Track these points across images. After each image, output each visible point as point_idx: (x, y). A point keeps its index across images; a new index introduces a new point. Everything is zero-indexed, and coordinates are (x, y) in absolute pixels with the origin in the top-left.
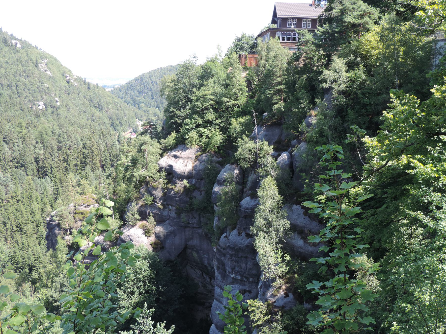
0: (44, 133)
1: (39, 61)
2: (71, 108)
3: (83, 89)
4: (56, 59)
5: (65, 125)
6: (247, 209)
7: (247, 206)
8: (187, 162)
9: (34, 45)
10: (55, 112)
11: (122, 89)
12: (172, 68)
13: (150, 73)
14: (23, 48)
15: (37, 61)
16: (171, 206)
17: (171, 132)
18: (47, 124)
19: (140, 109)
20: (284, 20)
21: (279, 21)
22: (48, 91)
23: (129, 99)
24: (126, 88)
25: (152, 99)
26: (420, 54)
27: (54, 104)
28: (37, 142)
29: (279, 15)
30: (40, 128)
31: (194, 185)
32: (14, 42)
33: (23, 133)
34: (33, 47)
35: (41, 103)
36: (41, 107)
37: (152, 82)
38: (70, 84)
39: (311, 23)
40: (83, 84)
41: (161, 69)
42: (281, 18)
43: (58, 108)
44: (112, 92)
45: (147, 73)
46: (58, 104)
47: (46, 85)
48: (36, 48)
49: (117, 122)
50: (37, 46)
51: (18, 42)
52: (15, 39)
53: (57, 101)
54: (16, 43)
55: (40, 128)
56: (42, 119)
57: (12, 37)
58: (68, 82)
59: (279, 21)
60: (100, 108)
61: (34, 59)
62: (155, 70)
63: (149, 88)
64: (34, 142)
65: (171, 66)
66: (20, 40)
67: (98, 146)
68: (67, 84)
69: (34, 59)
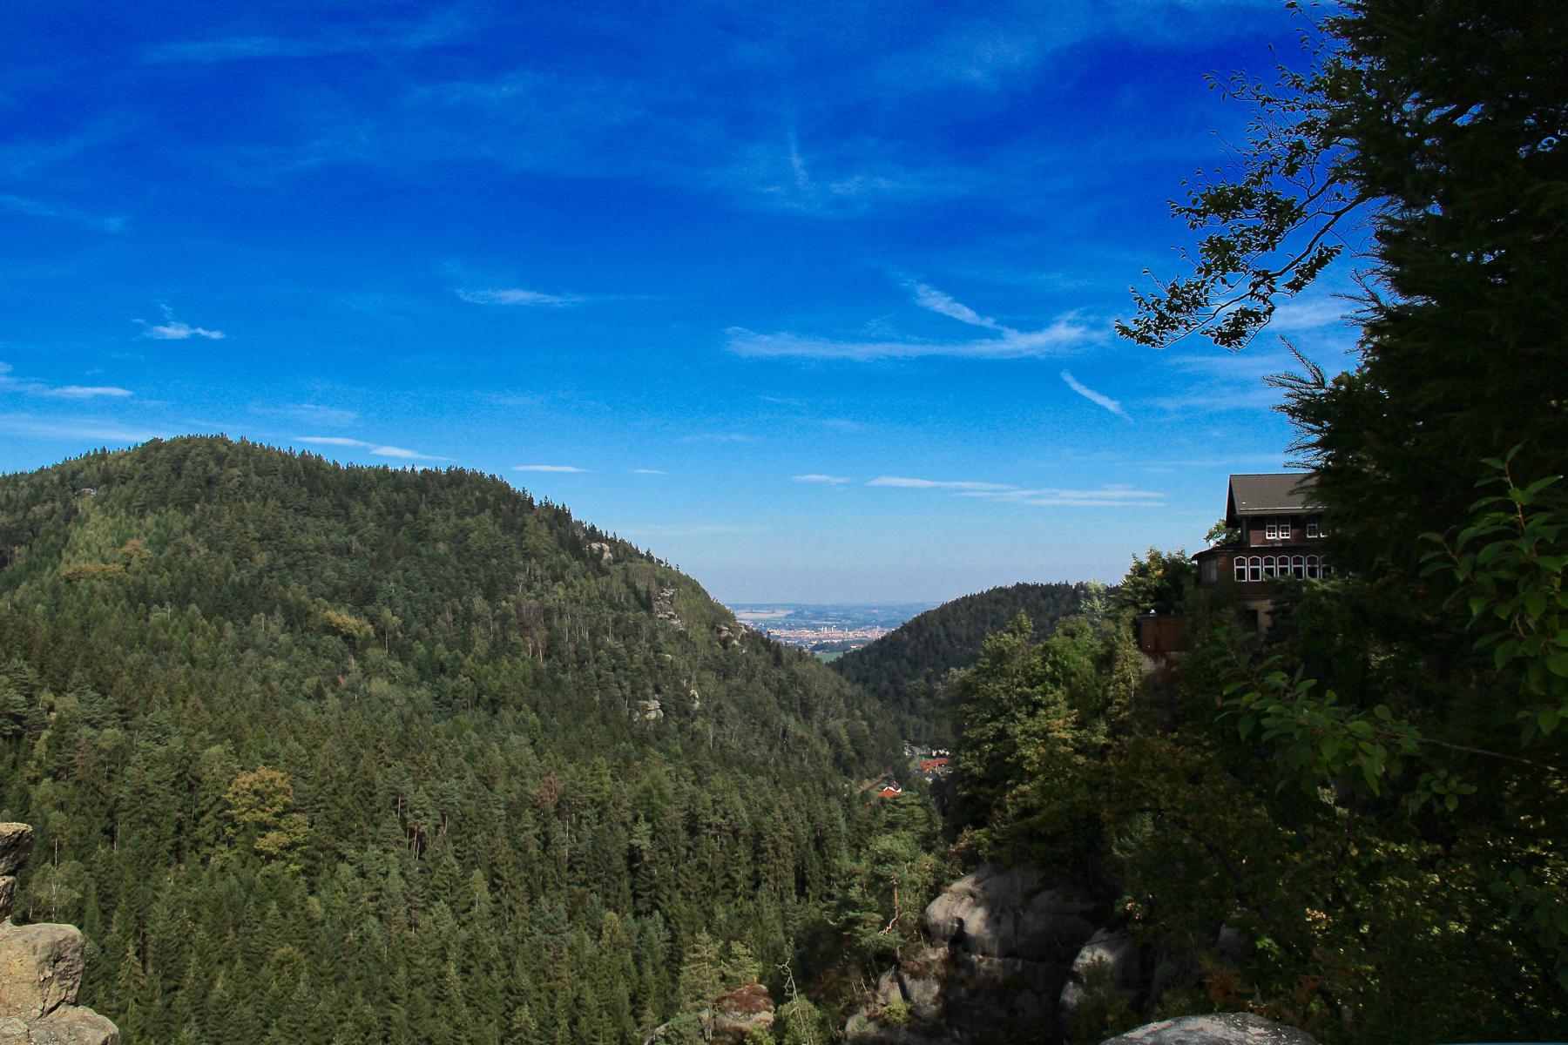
0: (655, 792)
3: (761, 662)
14: (617, 561)
16: (960, 1030)
23: (885, 683)
26: (1097, 970)
28: (636, 819)
30: (646, 781)
32: (595, 546)
35: (654, 704)
36: (653, 715)
37: (948, 636)
40: (763, 648)
41: (972, 598)
42: (1247, 517)
44: (839, 666)
48: (649, 558)
50: (653, 554)
51: (606, 547)
52: (600, 538)
54: (601, 550)
55: (646, 781)
57: (593, 535)
60: (806, 710)
64: (629, 817)
66: (612, 542)
67: (793, 830)
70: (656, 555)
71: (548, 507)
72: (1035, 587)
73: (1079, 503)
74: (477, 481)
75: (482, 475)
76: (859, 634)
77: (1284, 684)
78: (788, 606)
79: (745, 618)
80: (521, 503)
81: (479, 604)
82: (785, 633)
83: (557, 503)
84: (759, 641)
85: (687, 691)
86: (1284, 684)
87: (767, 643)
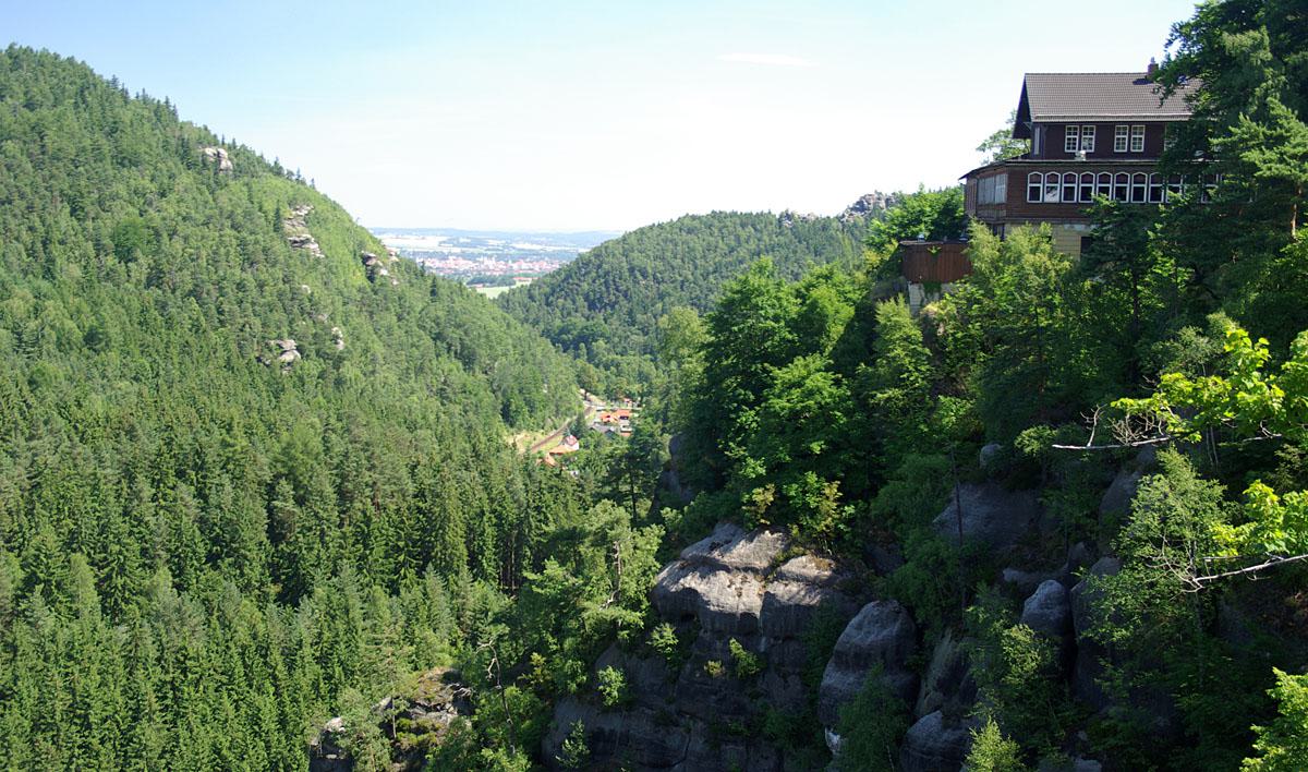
1: (287, 212)
2: (380, 357)
3: (417, 299)
4: (335, 207)
5: (362, 419)
6: (930, 753)
7: (930, 743)
8: (744, 581)
9: (270, 160)
10: (333, 375)
11: (536, 292)
12: (696, 223)
13: (624, 239)
15: (278, 210)
17: (697, 475)
18: (305, 424)
19: (591, 357)
20: (1055, 132)
21: (1037, 131)
22: (310, 309)
24: (548, 290)
25: (633, 323)
27: (327, 345)
29: (1038, 113)
31: (767, 654)
32: (210, 151)
33: (238, 448)
34: (268, 166)
35: (290, 344)
38: (378, 281)
39: (1143, 136)
41: (660, 226)
43: (338, 361)
44: (505, 302)
45: (618, 242)
46: (341, 345)
47: (306, 288)
49: (517, 402)
50: (281, 164)
51: (222, 151)
52: (214, 142)
53: (337, 337)
56: (291, 397)
58: (371, 278)
59: (1037, 131)
60: (467, 359)
61: (269, 206)
62: (642, 231)
63: (623, 288)
65: (694, 218)
66: (232, 147)
68: (367, 283)
69: (269, 206)
70: (286, 166)
71: (145, 100)
72: (734, 214)
73: (1017, 169)
74: (44, 63)
75: (56, 56)
76: (525, 266)
77: (283, 482)
78: (445, 231)
79: (391, 243)
80: (113, 93)
81: (64, 221)
82: (438, 264)
83: (158, 94)
84: (413, 271)
85: (327, 329)
86: (283, 482)
87: (421, 273)
